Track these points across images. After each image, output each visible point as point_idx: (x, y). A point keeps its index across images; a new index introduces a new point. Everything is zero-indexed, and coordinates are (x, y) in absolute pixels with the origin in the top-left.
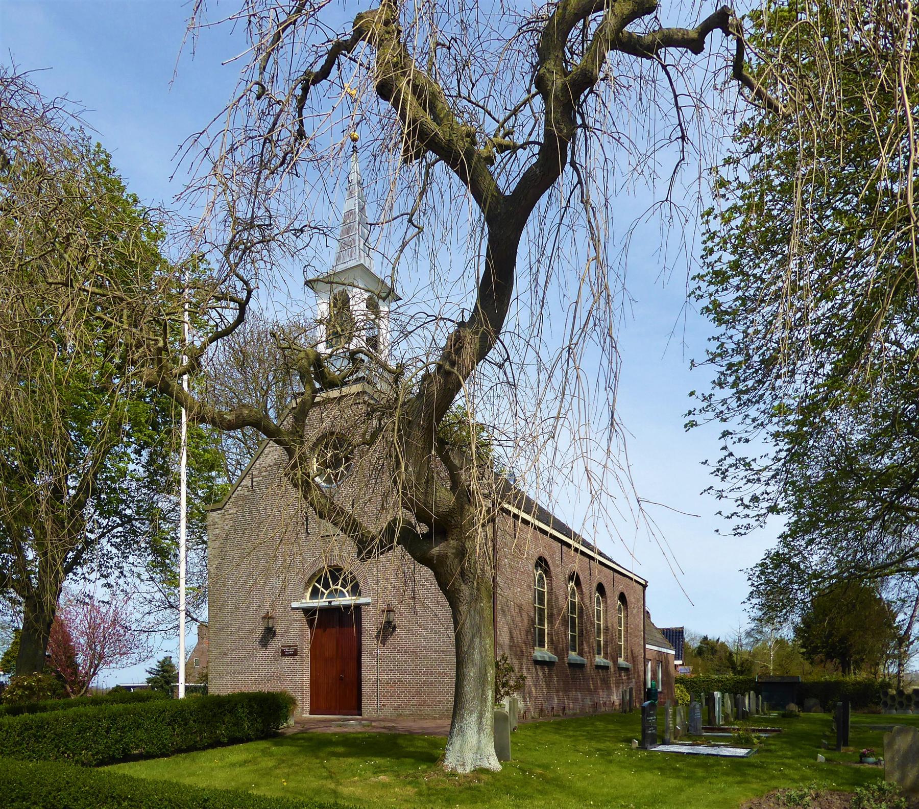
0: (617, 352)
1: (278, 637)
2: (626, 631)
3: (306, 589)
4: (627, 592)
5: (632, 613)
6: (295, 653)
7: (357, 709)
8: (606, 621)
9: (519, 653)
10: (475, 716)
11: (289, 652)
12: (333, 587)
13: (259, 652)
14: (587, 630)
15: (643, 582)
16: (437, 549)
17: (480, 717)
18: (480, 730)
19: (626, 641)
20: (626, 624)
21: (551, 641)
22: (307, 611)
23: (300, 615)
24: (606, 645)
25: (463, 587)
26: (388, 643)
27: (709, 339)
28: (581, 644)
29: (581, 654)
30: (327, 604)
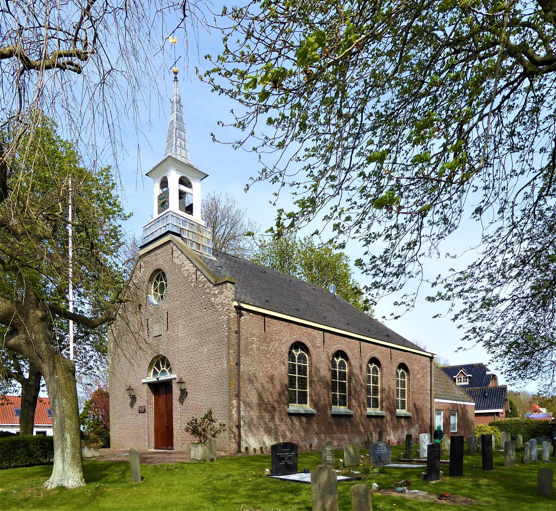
0: (504, 168)
1: (137, 402)
2: (409, 390)
3: (149, 370)
4: (482, 364)
5: (415, 377)
6: (144, 412)
7: (107, 445)
8: (382, 384)
9: (270, 408)
10: (60, 450)
11: (142, 411)
12: (162, 369)
13: (130, 411)
14: (355, 391)
15: (430, 355)
16: (13, 340)
17: (63, 452)
18: (64, 461)
19: (409, 397)
20: (409, 385)
21: (312, 400)
22: (150, 385)
23: (146, 387)
24: (382, 401)
25: (43, 365)
26: (185, 403)
27: (212, 135)
28: (350, 400)
29: (350, 408)
30: (156, 380)
